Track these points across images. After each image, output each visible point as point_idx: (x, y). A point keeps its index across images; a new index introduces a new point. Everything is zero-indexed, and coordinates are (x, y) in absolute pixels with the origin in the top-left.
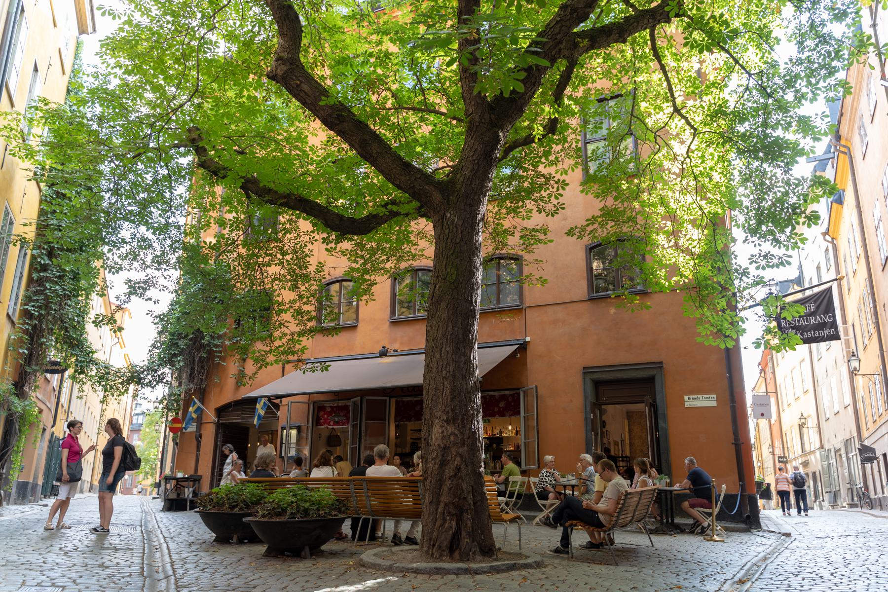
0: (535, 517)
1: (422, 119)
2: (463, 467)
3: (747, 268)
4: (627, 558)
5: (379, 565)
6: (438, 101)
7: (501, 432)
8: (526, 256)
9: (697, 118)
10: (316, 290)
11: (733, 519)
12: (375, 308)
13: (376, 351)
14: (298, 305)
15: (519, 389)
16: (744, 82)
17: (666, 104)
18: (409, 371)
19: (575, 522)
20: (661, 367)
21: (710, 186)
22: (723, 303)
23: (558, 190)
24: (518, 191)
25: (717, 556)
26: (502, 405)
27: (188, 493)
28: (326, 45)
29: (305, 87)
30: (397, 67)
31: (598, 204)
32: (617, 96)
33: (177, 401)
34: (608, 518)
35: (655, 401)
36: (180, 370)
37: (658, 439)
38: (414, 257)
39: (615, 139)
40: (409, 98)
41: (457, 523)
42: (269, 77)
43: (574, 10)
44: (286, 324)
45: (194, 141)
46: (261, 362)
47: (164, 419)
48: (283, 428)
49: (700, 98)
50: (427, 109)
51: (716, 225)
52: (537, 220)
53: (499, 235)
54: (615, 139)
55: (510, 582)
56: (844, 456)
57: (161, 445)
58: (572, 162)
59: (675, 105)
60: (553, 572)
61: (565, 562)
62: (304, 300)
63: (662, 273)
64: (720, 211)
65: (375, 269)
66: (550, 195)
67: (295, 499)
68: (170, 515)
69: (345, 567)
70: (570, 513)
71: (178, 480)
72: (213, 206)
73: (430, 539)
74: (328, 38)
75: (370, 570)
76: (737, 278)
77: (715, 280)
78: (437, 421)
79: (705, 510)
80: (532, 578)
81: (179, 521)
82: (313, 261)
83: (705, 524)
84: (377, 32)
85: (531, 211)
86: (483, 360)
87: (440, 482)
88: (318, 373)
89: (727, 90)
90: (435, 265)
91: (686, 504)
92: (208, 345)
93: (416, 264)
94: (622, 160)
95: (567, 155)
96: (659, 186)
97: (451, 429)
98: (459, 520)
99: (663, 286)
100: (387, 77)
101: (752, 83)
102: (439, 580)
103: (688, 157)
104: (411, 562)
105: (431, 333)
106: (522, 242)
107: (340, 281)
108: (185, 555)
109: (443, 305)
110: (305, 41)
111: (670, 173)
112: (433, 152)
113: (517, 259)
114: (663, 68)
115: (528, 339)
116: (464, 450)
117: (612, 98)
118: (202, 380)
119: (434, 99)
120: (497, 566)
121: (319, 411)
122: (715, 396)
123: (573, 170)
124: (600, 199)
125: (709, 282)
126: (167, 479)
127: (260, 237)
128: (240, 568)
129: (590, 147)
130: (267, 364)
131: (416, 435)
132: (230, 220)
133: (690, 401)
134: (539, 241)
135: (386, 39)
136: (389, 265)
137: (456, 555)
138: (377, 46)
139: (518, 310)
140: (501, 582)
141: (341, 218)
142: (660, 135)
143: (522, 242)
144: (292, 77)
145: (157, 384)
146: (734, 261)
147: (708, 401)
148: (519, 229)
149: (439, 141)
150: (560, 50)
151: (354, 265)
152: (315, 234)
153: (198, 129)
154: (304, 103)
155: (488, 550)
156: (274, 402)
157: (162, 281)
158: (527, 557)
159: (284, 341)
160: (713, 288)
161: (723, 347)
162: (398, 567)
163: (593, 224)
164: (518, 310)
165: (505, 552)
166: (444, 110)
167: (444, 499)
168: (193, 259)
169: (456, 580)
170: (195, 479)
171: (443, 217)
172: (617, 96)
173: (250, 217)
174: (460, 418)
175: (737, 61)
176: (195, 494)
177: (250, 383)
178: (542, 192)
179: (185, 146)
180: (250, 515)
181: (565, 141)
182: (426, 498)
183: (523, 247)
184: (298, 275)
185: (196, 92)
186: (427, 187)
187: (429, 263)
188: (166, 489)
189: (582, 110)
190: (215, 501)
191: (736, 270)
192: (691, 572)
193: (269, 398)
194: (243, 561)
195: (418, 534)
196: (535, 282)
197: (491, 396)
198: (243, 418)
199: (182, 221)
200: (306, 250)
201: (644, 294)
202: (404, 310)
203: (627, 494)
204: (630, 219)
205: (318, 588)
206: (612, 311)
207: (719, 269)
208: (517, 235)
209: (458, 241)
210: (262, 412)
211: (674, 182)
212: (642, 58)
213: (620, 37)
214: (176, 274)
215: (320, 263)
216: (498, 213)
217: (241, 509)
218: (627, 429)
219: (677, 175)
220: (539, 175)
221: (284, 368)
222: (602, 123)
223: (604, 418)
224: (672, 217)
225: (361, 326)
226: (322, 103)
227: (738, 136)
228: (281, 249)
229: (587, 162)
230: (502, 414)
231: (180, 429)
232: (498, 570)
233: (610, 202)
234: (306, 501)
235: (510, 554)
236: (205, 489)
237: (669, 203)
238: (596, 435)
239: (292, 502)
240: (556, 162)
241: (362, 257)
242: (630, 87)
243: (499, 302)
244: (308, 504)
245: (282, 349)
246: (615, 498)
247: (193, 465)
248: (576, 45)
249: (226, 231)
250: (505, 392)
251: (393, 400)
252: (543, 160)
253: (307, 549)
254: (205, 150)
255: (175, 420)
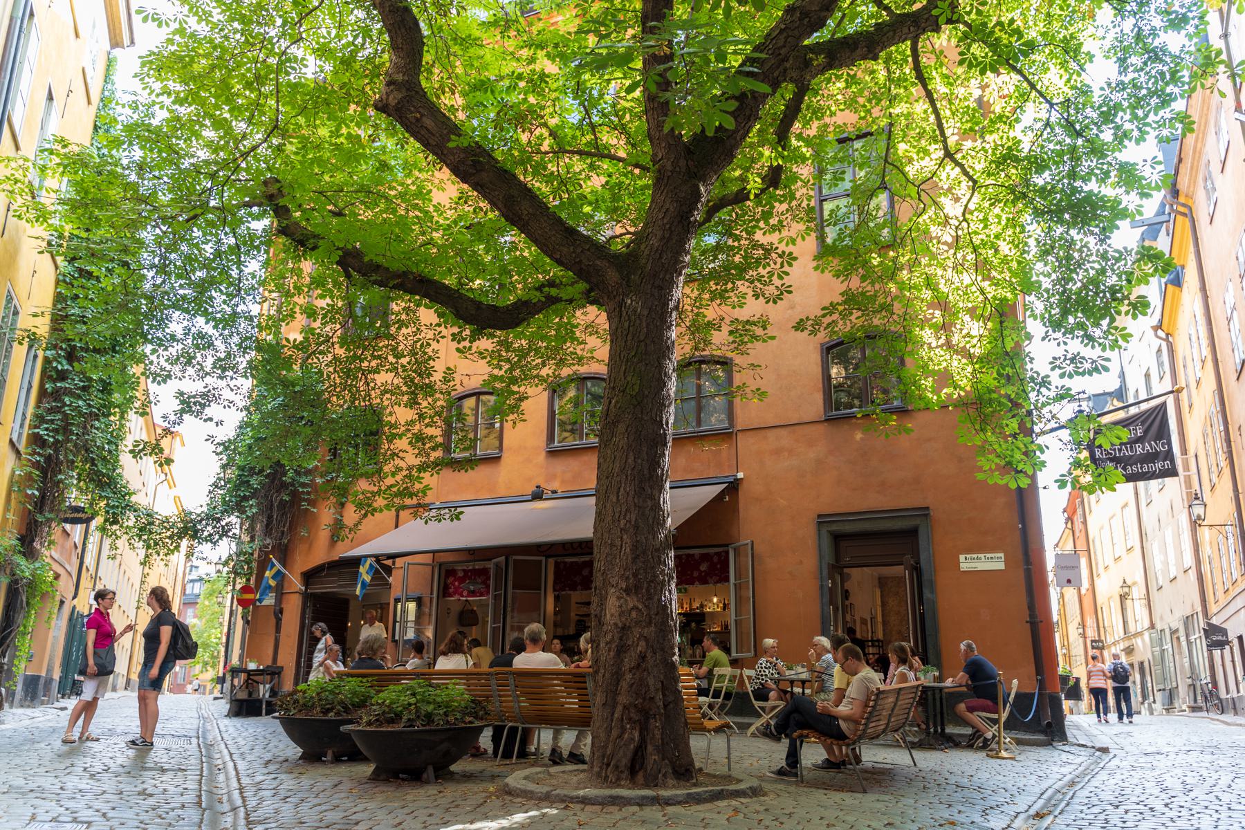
0: (750, 725)
1: (592, 167)
2: (649, 655)
3: (1048, 376)
4: (879, 782)
5: (532, 792)
6: (614, 141)
7: (702, 606)
8: (738, 360)
9: (978, 166)
10: (443, 407)
11: (1028, 728)
12: (526, 432)
13: (528, 493)
14: (417, 427)
15: (727, 545)
16: (1044, 115)
17: (934, 146)
18: (574, 520)
19: (805, 732)
20: (926, 515)
21: (996, 262)
22: (1014, 425)
23: (782, 266)
24: (727, 267)
25: (1006, 779)
26: (704, 567)
27: (263, 691)
28: (458, 63)
29: (428, 122)
30: (556, 94)
31: (839, 286)
32: (865, 135)
33: (248, 562)
34: (852, 726)
35: (918, 562)
36: (253, 519)
37: (922, 616)
38: (580, 360)
39: (862, 195)
40: (574, 137)
41: (641, 734)
42: (377, 108)
43: (805, 14)
44: (401, 454)
45: (272, 197)
46: (367, 509)
47: (230, 588)
48: (397, 600)
49: (982, 137)
50: (598, 152)
51: (1004, 315)
52: (753, 308)
53: (700, 329)
54: (862, 195)
55: (716, 816)
56: (1183, 639)
57: (226, 624)
58: (802, 227)
59: (946, 148)
60: (774, 802)
61: (792, 788)
62: (427, 421)
63: (928, 383)
64: (1009, 295)
65: (526, 378)
66: (771, 274)
67: (413, 700)
68: (238, 722)
69: (484, 795)
70: (799, 720)
71: (250, 673)
72: (298, 289)
73: (603, 756)
74: (460, 53)
75: (519, 800)
76: (1033, 390)
77: (1003, 392)
78: (613, 590)
79: (988, 715)
80: (746, 811)
81: (251, 731)
82: (439, 366)
83: (989, 735)
84: (529, 45)
85: (744, 296)
86: (678, 504)
87: (617, 676)
88: (446, 523)
89: (1019, 127)
90: (610, 372)
91: (962, 706)
92: (293, 485)
93: (583, 370)
94: (872, 225)
95: (794, 217)
96: (924, 261)
97: (632, 601)
98: (644, 730)
99: (929, 401)
100: (543, 108)
101: (1055, 116)
102: (615, 814)
103: (965, 220)
104: (577, 788)
105: (604, 467)
106: (731, 339)
107: (477, 394)
108: (259, 778)
109: (621, 427)
110: (427, 58)
111: (939, 242)
112: (607, 213)
113: (725, 363)
114: (929, 95)
115: (740, 475)
116: (650, 631)
117: (858, 137)
118: (283, 533)
119: (608, 138)
120: (697, 794)
121: (447, 577)
122: (1002, 555)
123: (803, 239)
124: (841, 279)
125: (994, 396)
126: (235, 672)
127: (365, 332)
128: (336, 796)
129: (828, 207)
130: (375, 510)
131: (584, 610)
132: (323, 309)
133: (967, 563)
134: (755, 338)
135: (541, 54)
136: (545, 371)
137: (640, 777)
138: (528, 64)
139: (726, 435)
140: (702, 816)
141: (478, 305)
142: (925, 190)
143: (731, 339)
144: (409, 107)
145: (220, 538)
146: (1029, 366)
147: (993, 562)
148: (727, 321)
149: (615, 198)
150: (785, 70)
151: (496, 372)
152: (442, 328)
153: (278, 181)
154: (427, 145)
155: (684, 771)
156: (384, 564)
157: (227, 394)
158: (739, 781)
159: (399, 477)
160: (1000, 403)
161: (1013, 486)
162: (558, 795)
163: (831, 314)
164: (726, 435)
165: (708, 774)
166: (622, 154)
167: (623, 699)
168: (270, 363)
169: (642, 813)
170: (274, 672)
171: (621, 304)
172: (865, 135)
173: (350, 304)
174: (644, 586)
175: (1033, 86)
176: (274, 693)
177: (350, 536)
178: (760, 269)
179: (260, 205)
180: (350, 722)
181: (793, 197)
182: (598, 699)
183: (732, 346)
184: (417, 386)
185: (275, 128)
186: (598, 262)
187: (603, 369)
188: (233, 685)
189: (817, 154)
190: (301, 702)
191: (1032, 379)
192: (968, 802)
193: (377, 558)
194: (340, 787)
195: (586, 748)
196: (750, 395)
197: (688, 556)
198: (341, 586)
199: (255, 309)
200: (429, 350)
201: (902, 412)
202: (566, 434)
203: (879, 692)
204: (883, 307)
205: (446, 824)
206: (859, 436)
207: (1008, 378)
208: (725, 329)
209: (642, 338)
210: (367, 578)
211: (945, 255)
212: (899, 82)
213: (869, 51)
214: (247, 384)
215: (448, 369)
216: (699, 298)
217: (338, 714)
218: (879, 602)
219: (950, 246)
220: (756, 245)
221: (397, 516)
222: (843, 172)
223: (847, 586)
224: (942, 304)
225: (507, 457)
226: (451, 145)
227: (1035, 191)
228: (394, 349)
229: (823, 228)
230: (704, 581)
231: (252, 602)
232: (698, 800)
233: (855, 283)
234: (429, 703)
235: (714, 776)
236: (288, 686)
237: (937, 284)
238: (836, 609)
239: (410, 704)
240: (779, 227)
241: (508, 360)
242: (884, 122)
243: (699, 423)
244: (432, 707)
245: (395, 489)
246: (862, 698)
247: (270, 651)
248: (807, 64)
249: (317, 324)
250: (708, 549)
251: (551, 561)
252: (761, 224)
253: (430, 770)
254: (287, 210)
255: (245, 589)
